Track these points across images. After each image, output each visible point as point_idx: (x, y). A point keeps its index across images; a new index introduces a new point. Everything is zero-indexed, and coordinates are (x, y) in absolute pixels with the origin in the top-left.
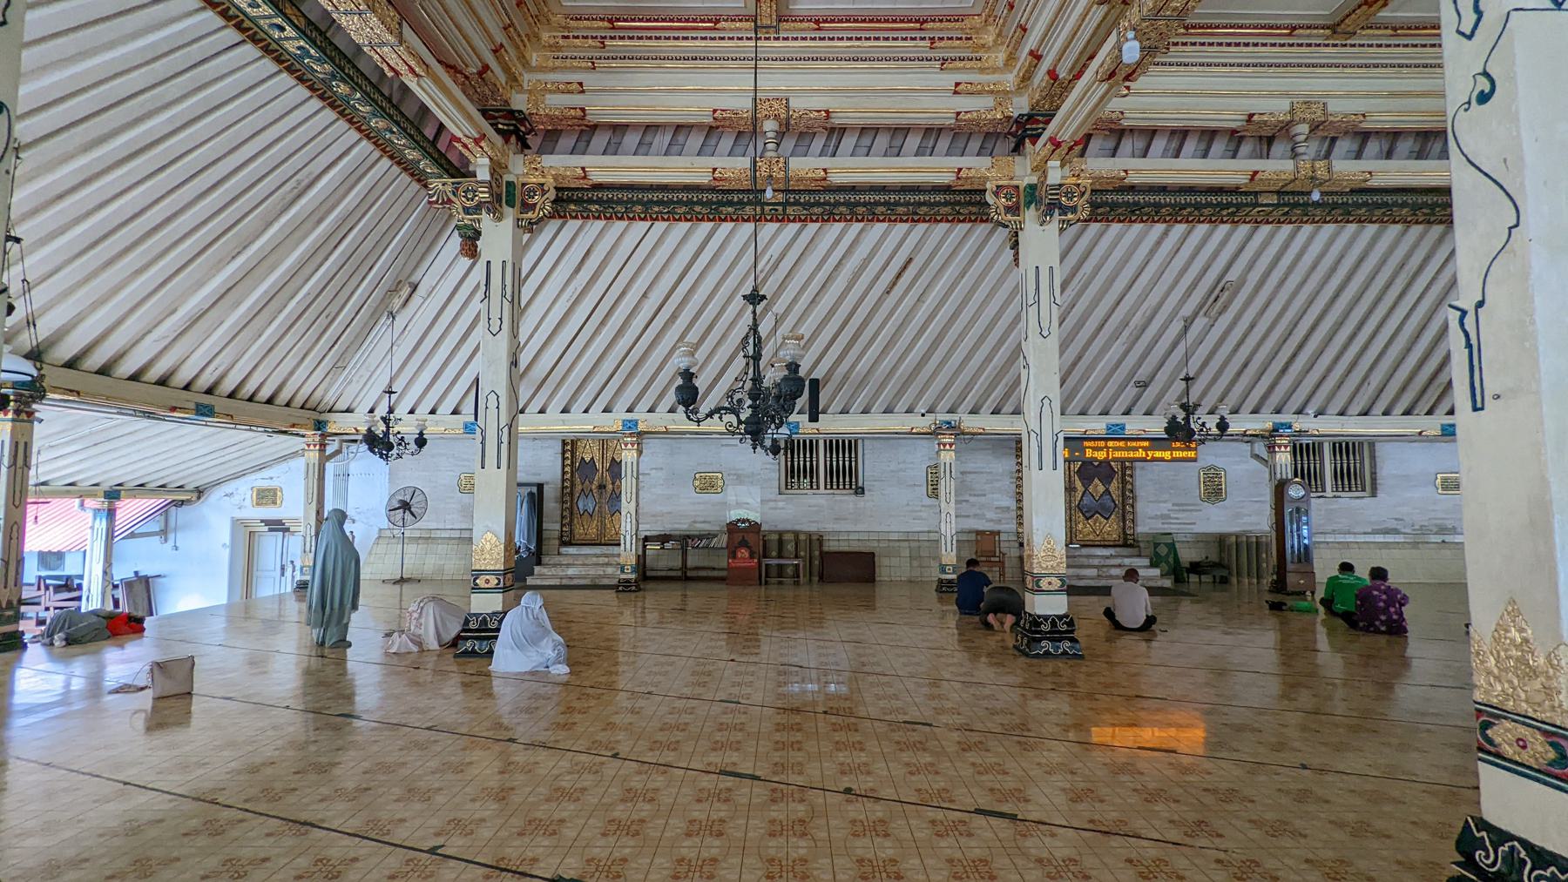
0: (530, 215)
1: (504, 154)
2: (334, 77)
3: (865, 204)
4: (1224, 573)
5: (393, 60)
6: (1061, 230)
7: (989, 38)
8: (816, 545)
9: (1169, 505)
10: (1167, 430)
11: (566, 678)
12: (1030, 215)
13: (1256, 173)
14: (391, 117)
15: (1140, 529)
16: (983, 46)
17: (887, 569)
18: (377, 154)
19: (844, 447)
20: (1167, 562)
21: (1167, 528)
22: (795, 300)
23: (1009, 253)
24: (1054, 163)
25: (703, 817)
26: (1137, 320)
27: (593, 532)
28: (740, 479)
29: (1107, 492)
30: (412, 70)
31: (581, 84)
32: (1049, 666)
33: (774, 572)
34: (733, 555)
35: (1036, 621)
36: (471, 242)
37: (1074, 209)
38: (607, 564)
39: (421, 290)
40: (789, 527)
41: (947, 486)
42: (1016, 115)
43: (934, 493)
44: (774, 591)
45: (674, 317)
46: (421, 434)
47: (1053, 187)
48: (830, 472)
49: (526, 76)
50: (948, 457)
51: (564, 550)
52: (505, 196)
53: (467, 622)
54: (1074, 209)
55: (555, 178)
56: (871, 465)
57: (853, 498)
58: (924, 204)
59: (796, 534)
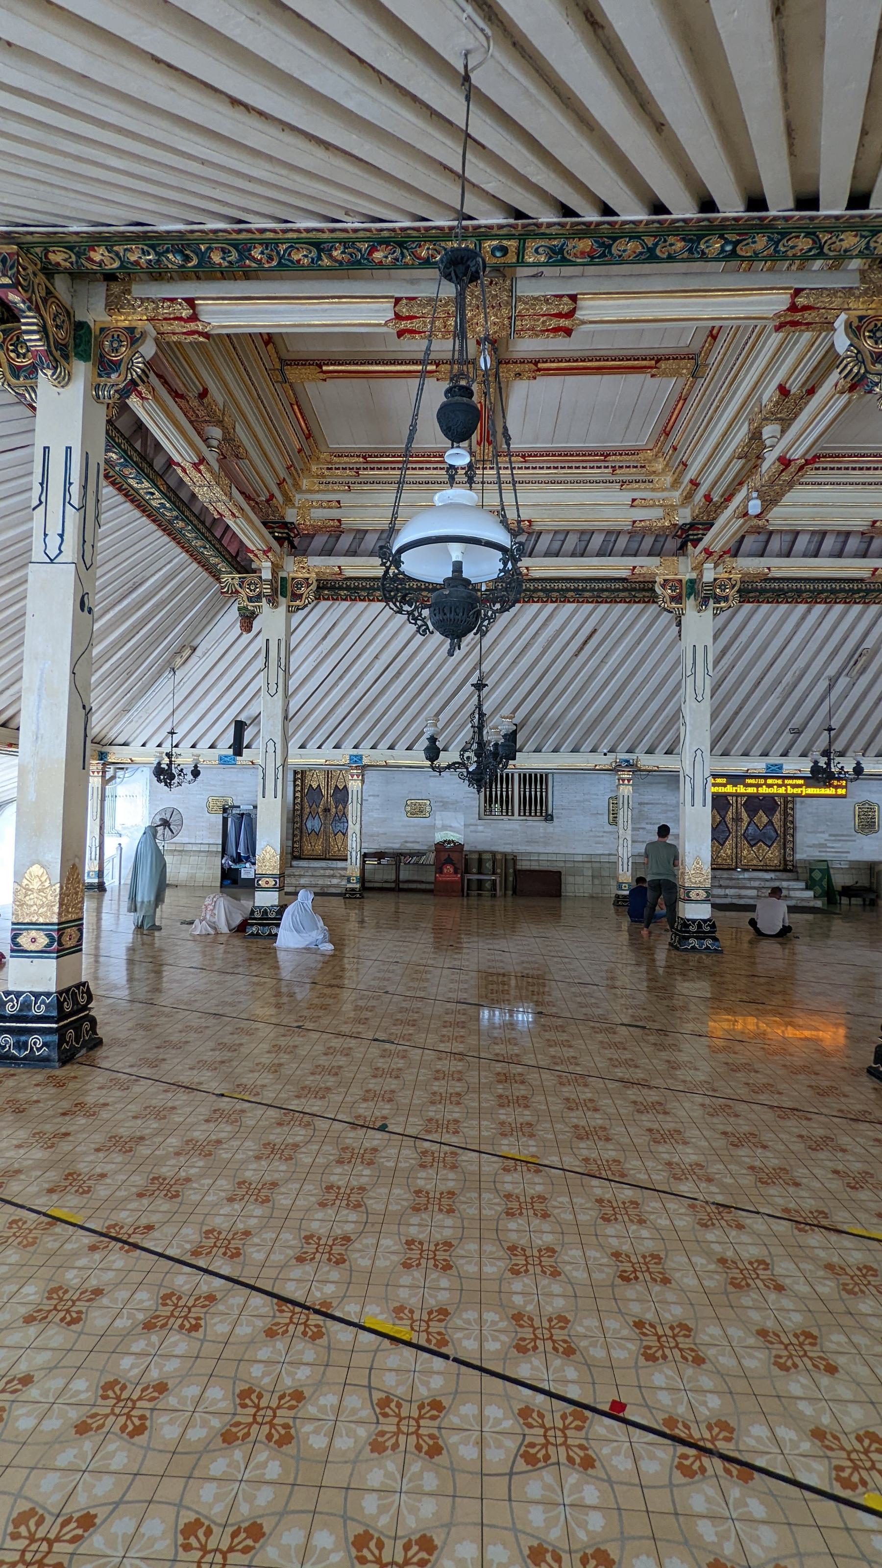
0: (298, 603)
1: (282, 558)
2: (177, 518)
3: (558, 590)
4: (873, 896)
5: (221, 508)
6: (715, 615)
7: (659, 466)
8: (510, 864)
9: (826, 836)
10: (812, 772)
11: (332, 953)
12: (690, 604)
13: (876, 569)
14: (207, 538)
15: (798, 856)
16: (654, 472)
17: (573, 886)
18: (190, 561)
19: (536, 781)
20: (821, 886)
21: (824, 856)
22: (499, 662)
23: (674, 629)
24: (709, 565)
25: (324, 1231)
26: (788, 678)
27: (319, 848)
28: (445, 805)
29: (770, 822)
30: (233, 515)
31: (339, 502)
32: (693, 958)
33: (474, 886)
34: (440, 870)
35: (686, 923)
36: (247, 620)
37: (726, 599)
38: (333, 876)
39: (199, 652)
40: (487, 848)
41: (624, 815)
42: (680, 523)
43: (614, 821)
44: (473, 901)
45: (399, 673)
46: (196, 767)
47: (707, 584)
48: (523, 801)
49: (298, 496)
50: (626, 790)
51: (295, 863)
52: (283, 590)
53: (252, 912)
54: (726, 599)
55: (317, 574)
56: (559, 796)
57: (544, 824)
58: (607, 590)
59: (494, 854)
